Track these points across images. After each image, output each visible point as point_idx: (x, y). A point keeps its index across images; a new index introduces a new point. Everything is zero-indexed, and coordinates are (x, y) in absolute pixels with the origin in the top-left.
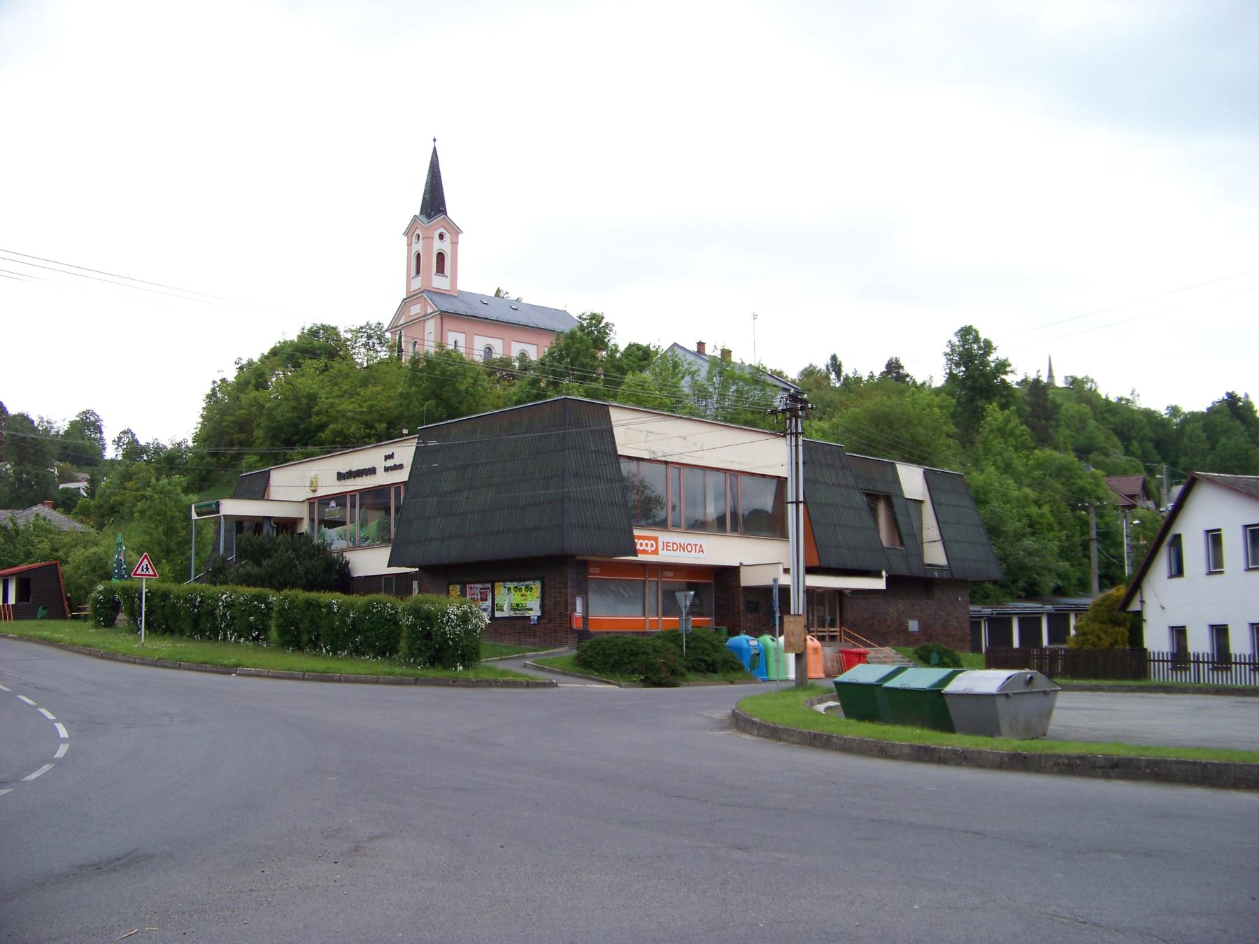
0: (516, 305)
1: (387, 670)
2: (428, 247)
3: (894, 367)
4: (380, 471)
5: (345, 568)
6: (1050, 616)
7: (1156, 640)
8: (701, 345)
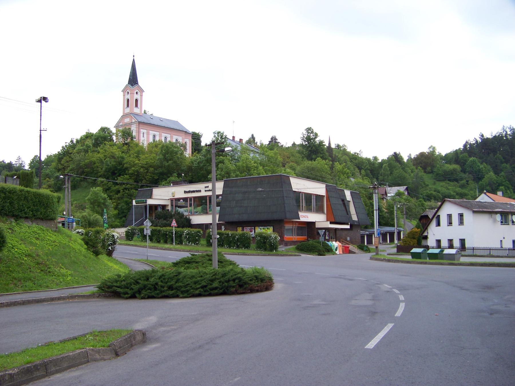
0: (152, 116)
1: (186, 255)
2: (132, 97)
3: (274, 140)
4: (203, 190)
5: (189, 220)
6: (367, 235)
8: (234, 137)
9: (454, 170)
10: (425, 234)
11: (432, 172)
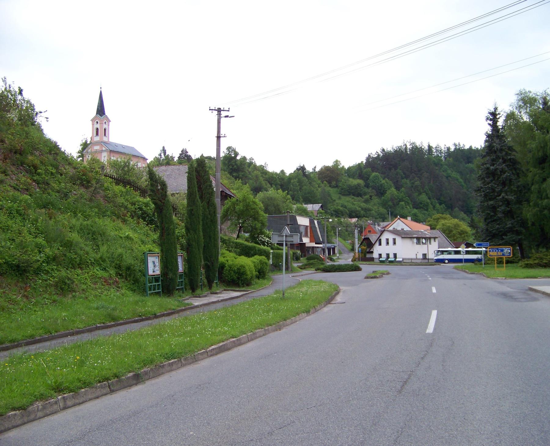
2: (102, 127)
7: (375, 255)
9: (359, 185)
10: (372, 250)
11: (337, 186)
